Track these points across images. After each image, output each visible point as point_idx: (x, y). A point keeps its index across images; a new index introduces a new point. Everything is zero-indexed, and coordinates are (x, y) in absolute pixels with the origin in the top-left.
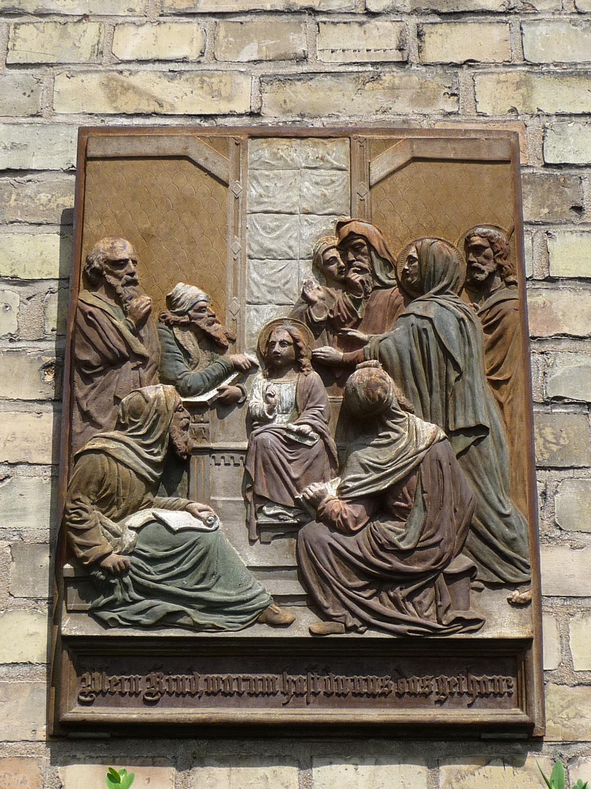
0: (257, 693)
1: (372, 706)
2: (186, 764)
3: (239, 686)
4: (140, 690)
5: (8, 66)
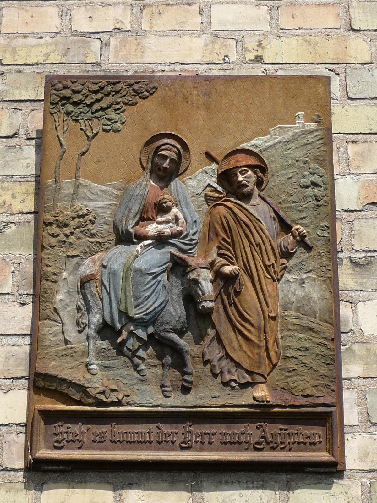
0: (131, 441)
2: (196, 488)
4: (152, 440)
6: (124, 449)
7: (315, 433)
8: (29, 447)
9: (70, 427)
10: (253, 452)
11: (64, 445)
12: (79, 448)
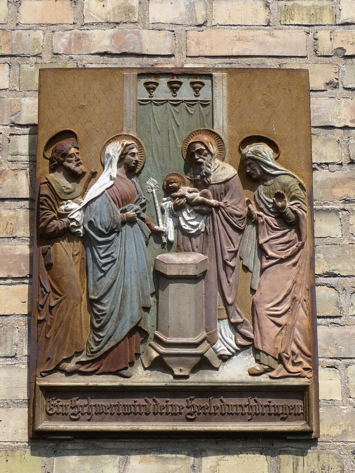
1: (232, 420)
3: (135, 409)
5: (187, 57)
6: (134, 421)
7: (252, 406)
8: (32, 420)
9: (169, 401)
10: (186, 422)
11: (196, 417)
12: (89, 420)
